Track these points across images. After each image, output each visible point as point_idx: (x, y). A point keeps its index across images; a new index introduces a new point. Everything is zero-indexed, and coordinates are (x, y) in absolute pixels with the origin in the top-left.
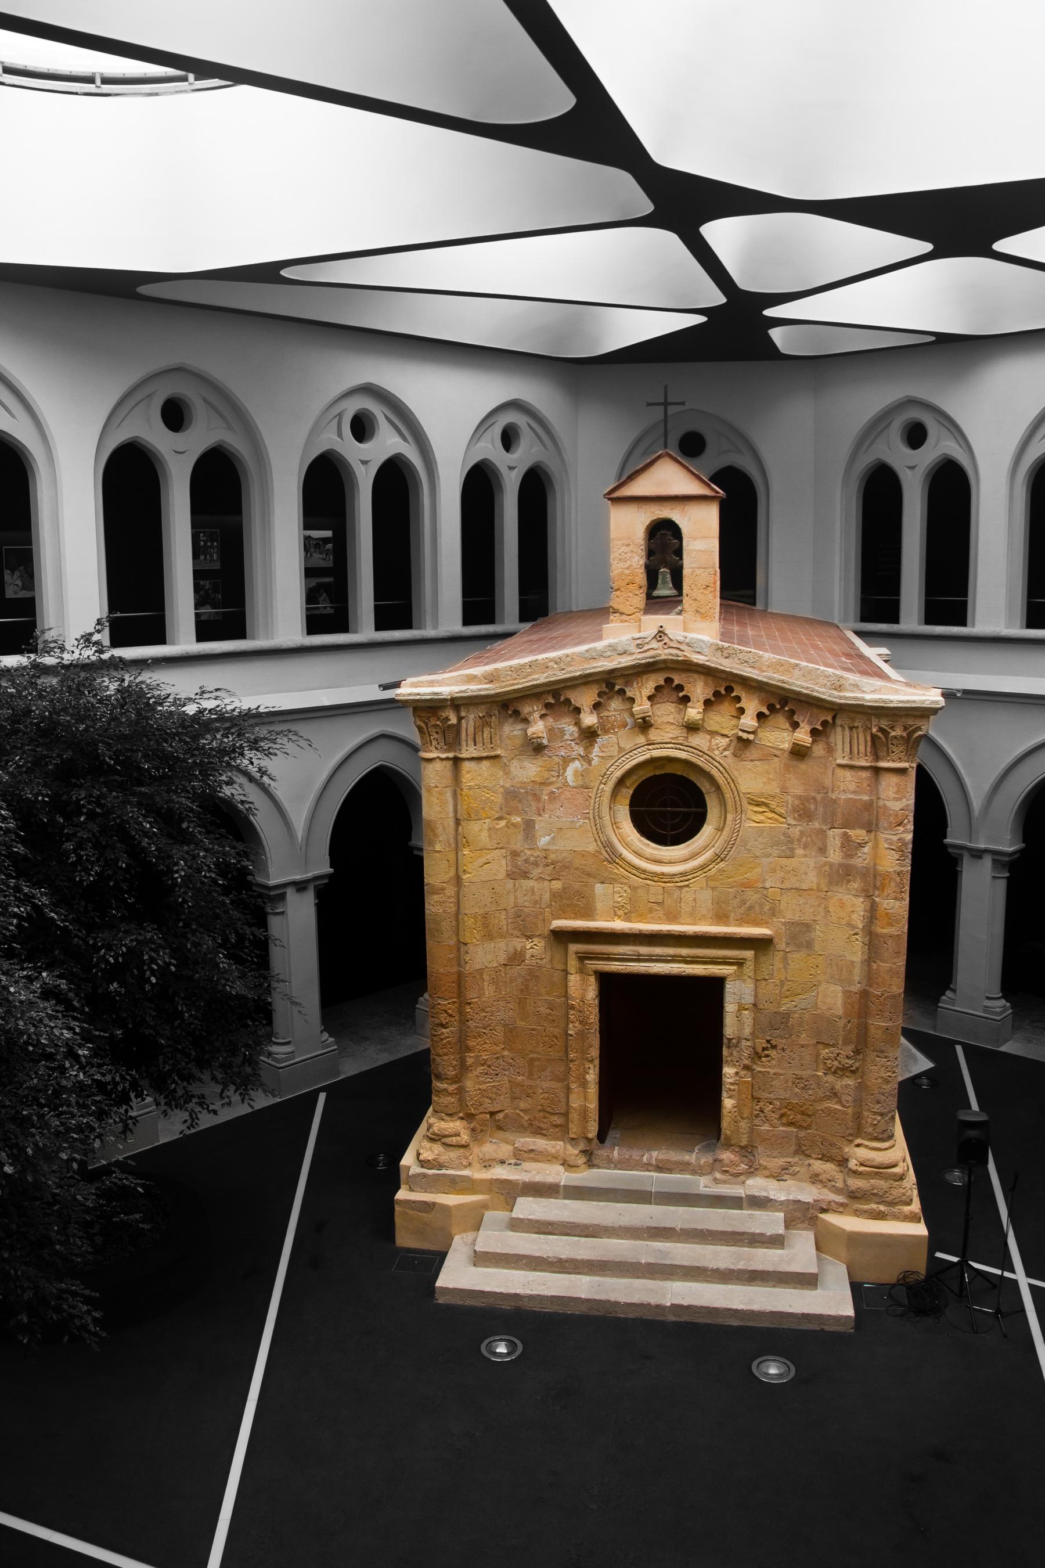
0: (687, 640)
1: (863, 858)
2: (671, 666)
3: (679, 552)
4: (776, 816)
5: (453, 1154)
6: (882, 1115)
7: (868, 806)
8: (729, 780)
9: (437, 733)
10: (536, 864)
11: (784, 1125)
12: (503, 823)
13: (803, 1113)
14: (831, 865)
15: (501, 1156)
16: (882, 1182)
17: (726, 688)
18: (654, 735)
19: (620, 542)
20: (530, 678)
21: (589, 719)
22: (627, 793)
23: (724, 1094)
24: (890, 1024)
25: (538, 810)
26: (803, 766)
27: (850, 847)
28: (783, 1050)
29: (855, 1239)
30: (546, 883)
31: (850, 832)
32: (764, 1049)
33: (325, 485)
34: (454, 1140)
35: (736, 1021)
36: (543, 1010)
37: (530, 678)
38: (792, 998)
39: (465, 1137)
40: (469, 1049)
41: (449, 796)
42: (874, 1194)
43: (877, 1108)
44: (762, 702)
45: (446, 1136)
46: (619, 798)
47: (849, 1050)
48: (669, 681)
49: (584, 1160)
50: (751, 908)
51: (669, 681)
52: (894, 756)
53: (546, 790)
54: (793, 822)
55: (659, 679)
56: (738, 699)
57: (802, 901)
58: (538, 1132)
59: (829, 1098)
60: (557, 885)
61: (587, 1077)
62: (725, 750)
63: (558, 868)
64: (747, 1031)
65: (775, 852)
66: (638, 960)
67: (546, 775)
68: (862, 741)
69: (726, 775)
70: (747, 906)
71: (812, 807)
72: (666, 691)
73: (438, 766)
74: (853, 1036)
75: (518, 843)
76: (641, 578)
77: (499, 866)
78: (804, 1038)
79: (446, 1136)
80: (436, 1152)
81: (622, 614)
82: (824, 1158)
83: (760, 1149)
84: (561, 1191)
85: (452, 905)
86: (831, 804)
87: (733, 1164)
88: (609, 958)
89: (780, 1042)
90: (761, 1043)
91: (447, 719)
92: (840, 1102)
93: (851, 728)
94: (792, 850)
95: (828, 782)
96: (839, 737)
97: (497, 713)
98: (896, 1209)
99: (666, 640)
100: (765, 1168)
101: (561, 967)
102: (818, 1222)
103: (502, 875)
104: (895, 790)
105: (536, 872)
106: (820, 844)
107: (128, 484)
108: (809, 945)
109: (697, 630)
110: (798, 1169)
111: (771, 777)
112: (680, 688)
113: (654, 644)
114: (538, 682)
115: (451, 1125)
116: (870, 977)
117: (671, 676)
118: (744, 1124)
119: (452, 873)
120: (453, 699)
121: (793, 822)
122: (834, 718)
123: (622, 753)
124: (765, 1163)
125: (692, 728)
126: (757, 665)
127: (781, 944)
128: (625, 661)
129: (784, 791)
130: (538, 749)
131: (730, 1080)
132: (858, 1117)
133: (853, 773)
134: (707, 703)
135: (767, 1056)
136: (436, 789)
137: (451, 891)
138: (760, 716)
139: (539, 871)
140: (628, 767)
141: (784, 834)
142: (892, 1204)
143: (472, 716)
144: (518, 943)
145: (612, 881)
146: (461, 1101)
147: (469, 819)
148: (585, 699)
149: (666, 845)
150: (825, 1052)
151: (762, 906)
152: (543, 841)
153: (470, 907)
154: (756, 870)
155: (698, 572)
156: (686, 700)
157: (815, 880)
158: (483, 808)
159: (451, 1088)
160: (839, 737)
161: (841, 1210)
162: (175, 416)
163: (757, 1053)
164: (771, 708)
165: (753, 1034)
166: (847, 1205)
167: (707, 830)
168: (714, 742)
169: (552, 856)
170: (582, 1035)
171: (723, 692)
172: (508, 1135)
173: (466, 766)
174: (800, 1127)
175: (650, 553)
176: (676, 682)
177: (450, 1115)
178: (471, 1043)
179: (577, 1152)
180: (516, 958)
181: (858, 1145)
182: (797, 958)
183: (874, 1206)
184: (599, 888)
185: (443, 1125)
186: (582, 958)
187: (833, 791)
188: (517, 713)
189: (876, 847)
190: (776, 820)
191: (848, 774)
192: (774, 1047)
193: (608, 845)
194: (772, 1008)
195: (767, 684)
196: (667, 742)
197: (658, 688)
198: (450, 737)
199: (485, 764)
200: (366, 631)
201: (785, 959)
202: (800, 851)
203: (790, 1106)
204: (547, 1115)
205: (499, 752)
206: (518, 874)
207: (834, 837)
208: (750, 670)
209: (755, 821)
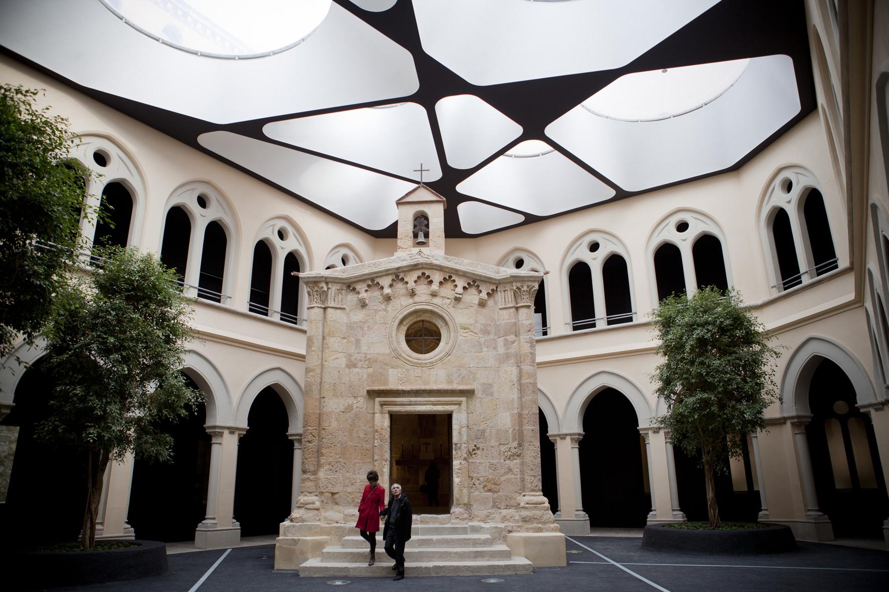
1: (513, 349)
3: (427, 226)
5: (311, 514)
7: (515, 324)
13: (495, 484)
14: (499, 355)
17: (450, 276)
18: (416, 299)
21: (387, 291)
22: (404, 329)
23: (454, 476)
26: (484, 311)
27: (507, 344)
29: (527, 541)
31: (508, 338)
33: (263, 254)
34: (311, 506)
36: (362, 435)
39: (318, 504)
40: (323, 455)
41: (320, 325)
43: (532, 473)
47: (515, 444)
48: (423, 274)
51: (423, 274)
53: (366, 325)
55: (419, 273)
59: (507, 473)
60: (370, 370)
63: (370, 362)
64: (465, 438)
66: (410, 405)
68: (510, 294)
72: (422, 279)
73: (316, 310)
74: (517, 437)
75: (352, 350)
76: (411, 235)
77: (342, 362)
78: (493, 443)
82: (507, 507)
83: (475, 506)
87: (462, 514)
88: (395, 404)
90: (472, 447)
95: (496, 318)
96: (499, 296)
98: (547, 526)
101: (371, 411)
103: (343, 366)
105: (360, 364)
107: (177, 223)
108: (492, 394)
109: (437, 250)
112: (428, 277)
113: (417, 256)
116: (522, 407)
117: (424, 271)
118: (465, 491)
119: (319, 362)
120: (326, 278)
123: (403, 305)
125: (434, 295)
127: (479, 394)
128: (404, 264)
129: (476, 322)
130: (363, 305)
132: (523, 480)
134: (441, 283)
137: (318, 371)
138: (465, 288)
140: (405, 313)
142: (544, 523)
143: (333, 289)
144: (351, 401)
145: (397, 367)
146: (317, 486)
147: (329, 335)
148: (385, 282)
149: (421, 353)
150: (503, 448)
152: (364, 349)
153: (327, 378)
156: (431, 282)
159: (312, 477)
162: (202, 202)
164: (469, 284)
167: (442, 344)
169: (368, 356)
170: (381, 447)
172: (340, 508)
173: (329, 310)
175: (415, 226)
178: (324, 451)
180: (349, 408)
184: (391, 370)
185: (306, 498)
188: (354, 289)
189: (519, 344)
191: (504, 312)
192: (478, 449)
194: (476, 428)
195: (467, 272)
196: (423, 298)
197: (419, 277)
198: (323, 297)
200: (276, 318)
201: (481, 402)
202: (485, 349)
206: (351, 365)
207: (500, 342)
209: (462, 336)
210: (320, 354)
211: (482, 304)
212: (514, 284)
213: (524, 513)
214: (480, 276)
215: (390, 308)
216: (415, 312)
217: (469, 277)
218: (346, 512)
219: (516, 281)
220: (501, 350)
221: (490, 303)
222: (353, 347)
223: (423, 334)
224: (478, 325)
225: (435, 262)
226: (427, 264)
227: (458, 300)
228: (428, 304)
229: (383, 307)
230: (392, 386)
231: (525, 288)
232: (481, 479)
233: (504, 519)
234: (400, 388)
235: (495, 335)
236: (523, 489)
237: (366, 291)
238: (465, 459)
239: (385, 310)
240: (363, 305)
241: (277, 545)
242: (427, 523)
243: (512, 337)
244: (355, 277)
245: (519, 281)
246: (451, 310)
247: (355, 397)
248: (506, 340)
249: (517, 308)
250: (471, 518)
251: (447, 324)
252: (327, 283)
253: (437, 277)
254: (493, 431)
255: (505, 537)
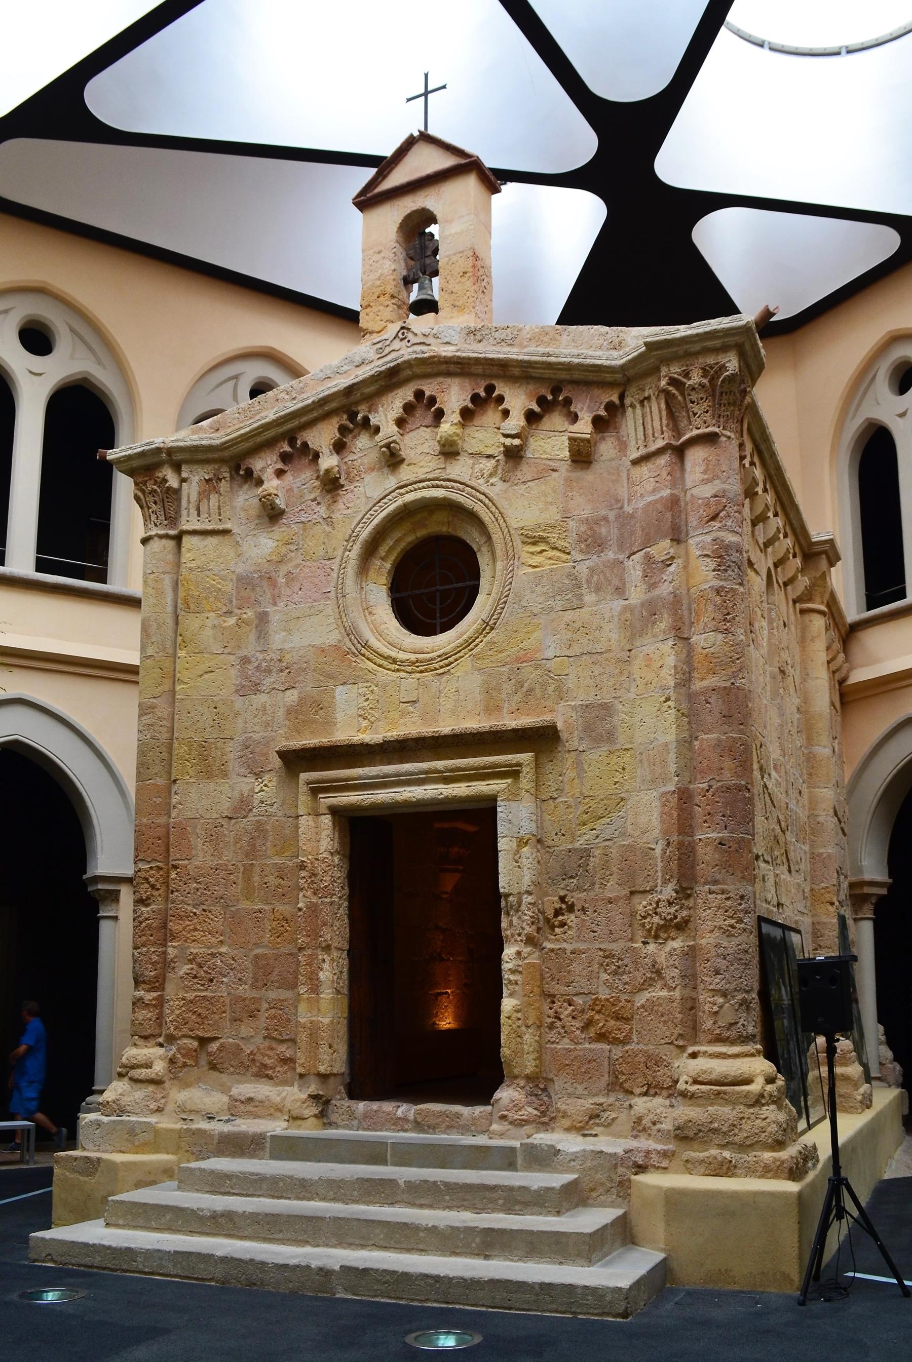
0: (434, 331)
2: (417, 370)
4: (558, 554)
6: (724, 995)
8: (487, 501)
9: (155, 503)
10: (268, 671)
11: (592, 1040)
12: (232, 621)
13: (618, 1017)
15: (213, 1109)
16: (727, 1109)
18: (406, 474)
19: (371, 251)
20: (258, 417)
21: (328, 461)
22: (382, 568)
24: (725, 834)
25: (274, 597)
27: (653, 569)
28: (584, 910)
29: (675, 1201)
30: (281, 694)
31: (653, 551)
32: (558, 912)
34: (143, 1073)
35: (515, 871)
37: (258, 417)
38: (590, 825)
42: (715, 1131)
43: (717, 982)
44: (529, 396)
45: (133, 1067)
46: (372, 574)
47: (669, 892)
48: (419, 394)
49: (315, 1110)
50: (530, 691)
51: (419, 394)
52: (698, 421)
53: (284, 569)
54: (579, 557)
55: (405, 395)
56: (501, 399)
57: (597, 670)
58: (263, 1074)
59: (648, 983)
60: (292, 696)
61: (321, 974)
62: (491, 475)
65: (558, 604)
67: (284, 550)
68: (657, 408)
69: (493, 509)
70: (524, 689)
71: (603, 530)
72: (419, 413)
74: (674, 865)
78: (613, 889)
79: (133, 1067)
80: (120, 1091)
81: (371, 333)
82: (651, 1090)
83: (558, 1084)
84: (268, 1145)
85: (164, 730)
86: (625, 519)
89: (575, 898)
90: (551, 902)
91: (165, 481)
92: (665, 986)
93: (642, 403)
94: (580, 597)
95: (623, 492)
96: (631, 423)
97: (227, 475)
98: (750, 1157)
99: (410, 336)
100: (565, 1115)
102: (633, 1191)
104: (703, 468)
105: (268, 681)
106: (616, 582)
108: (610, 737)
110: (614, 1115)
111: (549, 500)
112: (433, 400)
113: (397, 344)
114: (267, 420)
115: (145, 1051)
118: (529, 1037)
119: (167, 686)
120: (170, 451)
121: (579, 557)
122: (622, 397)
123: (372, 496)
124: (564, 1107)
125: (449, 451)
126: (517, 342)
127: (572, 739)
128: (364, 373)
130: (272, 514)
131: (509, 966)
132: (691, 1006)
133: (650, 465)
135: (563, 924)
136: (152, 576)
139: (272, 680)
141: (569, 575)
142: (743, 1147)
148: (321, 437)
151: (544, 685)
154: (535, 635)
155: (454, 259)
157: (614, 636)
158: (206, 598)
160: (630, 423)
161: (664, 1164)
163: (547, 920)
164: (541, 401)
165: (537, 884)
166: (673, 1153)
168: (478, 467)
171: (483, 394)
173: (187, 541)
174: (616, 1041)
176: (427, 393)
177: (146, 1038)
179: (304, 1096)
180: (243, 806)
181: (694, 1055)
182: (595, 757)
183: (714, 1152)
186: (316, 790)
187: (629, 501)
188: (249, 473)
190: (558, 559)
191: (645, 470)
192: (571, 908)
193: (351, 632)
195: (529, 364)
197: (408, 408)
199: (212, 541)
201: (578, 764)
203: (597, 1005)
204: (274, 1045)
205: (228, 526)
207: (634, 568)
208: (508, 349)
209: (532, 564)
210: (167, 664)
211: (582, 456)
212: (664, 370)
213: (686, 1112)
214: (568, 367)
215: (341, 510)
216: (405, 514)
217: (539, 380)
218: (235, 1091)
219: (667, 361)
220: (637, 594)
221: (606, 448)
222: (252, 637)
223: (433, 574)
224: (572, 524)
225: (447, 351)
226: (423, 362)
227: (514, 455)
228: (436, 482)
229: (322, 510)
230: (346, 732)
231: (696, 378)
232: (579, 1000)
233: (639, 1127)
234: (368, 737)
235: (621, 547)
236: (690, 1033)
237: (280, 473)
238: (530, 941)
239: (328, 520)
240: (272, 514)
241: (56, 1171)
242: (433, 1128)
243: (663, 548)
244: (245, 437)
245: (675, 358)
246: (496, 489)
247: (258, 775)
248: (649, 559)
249: (679, 452)
250: (546, 1119)
251: (489, 538)
252: (177, 467)
253: (454, 396)
254: (614, 852)
255: (624, 1186)
